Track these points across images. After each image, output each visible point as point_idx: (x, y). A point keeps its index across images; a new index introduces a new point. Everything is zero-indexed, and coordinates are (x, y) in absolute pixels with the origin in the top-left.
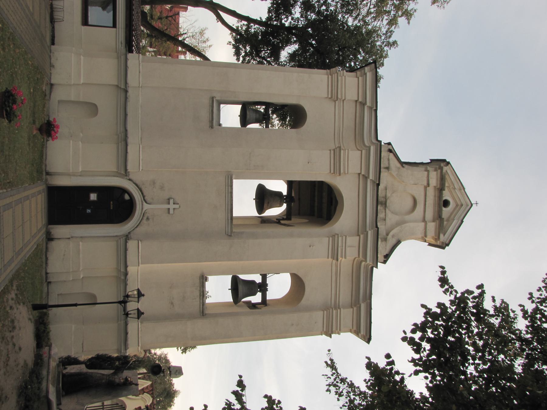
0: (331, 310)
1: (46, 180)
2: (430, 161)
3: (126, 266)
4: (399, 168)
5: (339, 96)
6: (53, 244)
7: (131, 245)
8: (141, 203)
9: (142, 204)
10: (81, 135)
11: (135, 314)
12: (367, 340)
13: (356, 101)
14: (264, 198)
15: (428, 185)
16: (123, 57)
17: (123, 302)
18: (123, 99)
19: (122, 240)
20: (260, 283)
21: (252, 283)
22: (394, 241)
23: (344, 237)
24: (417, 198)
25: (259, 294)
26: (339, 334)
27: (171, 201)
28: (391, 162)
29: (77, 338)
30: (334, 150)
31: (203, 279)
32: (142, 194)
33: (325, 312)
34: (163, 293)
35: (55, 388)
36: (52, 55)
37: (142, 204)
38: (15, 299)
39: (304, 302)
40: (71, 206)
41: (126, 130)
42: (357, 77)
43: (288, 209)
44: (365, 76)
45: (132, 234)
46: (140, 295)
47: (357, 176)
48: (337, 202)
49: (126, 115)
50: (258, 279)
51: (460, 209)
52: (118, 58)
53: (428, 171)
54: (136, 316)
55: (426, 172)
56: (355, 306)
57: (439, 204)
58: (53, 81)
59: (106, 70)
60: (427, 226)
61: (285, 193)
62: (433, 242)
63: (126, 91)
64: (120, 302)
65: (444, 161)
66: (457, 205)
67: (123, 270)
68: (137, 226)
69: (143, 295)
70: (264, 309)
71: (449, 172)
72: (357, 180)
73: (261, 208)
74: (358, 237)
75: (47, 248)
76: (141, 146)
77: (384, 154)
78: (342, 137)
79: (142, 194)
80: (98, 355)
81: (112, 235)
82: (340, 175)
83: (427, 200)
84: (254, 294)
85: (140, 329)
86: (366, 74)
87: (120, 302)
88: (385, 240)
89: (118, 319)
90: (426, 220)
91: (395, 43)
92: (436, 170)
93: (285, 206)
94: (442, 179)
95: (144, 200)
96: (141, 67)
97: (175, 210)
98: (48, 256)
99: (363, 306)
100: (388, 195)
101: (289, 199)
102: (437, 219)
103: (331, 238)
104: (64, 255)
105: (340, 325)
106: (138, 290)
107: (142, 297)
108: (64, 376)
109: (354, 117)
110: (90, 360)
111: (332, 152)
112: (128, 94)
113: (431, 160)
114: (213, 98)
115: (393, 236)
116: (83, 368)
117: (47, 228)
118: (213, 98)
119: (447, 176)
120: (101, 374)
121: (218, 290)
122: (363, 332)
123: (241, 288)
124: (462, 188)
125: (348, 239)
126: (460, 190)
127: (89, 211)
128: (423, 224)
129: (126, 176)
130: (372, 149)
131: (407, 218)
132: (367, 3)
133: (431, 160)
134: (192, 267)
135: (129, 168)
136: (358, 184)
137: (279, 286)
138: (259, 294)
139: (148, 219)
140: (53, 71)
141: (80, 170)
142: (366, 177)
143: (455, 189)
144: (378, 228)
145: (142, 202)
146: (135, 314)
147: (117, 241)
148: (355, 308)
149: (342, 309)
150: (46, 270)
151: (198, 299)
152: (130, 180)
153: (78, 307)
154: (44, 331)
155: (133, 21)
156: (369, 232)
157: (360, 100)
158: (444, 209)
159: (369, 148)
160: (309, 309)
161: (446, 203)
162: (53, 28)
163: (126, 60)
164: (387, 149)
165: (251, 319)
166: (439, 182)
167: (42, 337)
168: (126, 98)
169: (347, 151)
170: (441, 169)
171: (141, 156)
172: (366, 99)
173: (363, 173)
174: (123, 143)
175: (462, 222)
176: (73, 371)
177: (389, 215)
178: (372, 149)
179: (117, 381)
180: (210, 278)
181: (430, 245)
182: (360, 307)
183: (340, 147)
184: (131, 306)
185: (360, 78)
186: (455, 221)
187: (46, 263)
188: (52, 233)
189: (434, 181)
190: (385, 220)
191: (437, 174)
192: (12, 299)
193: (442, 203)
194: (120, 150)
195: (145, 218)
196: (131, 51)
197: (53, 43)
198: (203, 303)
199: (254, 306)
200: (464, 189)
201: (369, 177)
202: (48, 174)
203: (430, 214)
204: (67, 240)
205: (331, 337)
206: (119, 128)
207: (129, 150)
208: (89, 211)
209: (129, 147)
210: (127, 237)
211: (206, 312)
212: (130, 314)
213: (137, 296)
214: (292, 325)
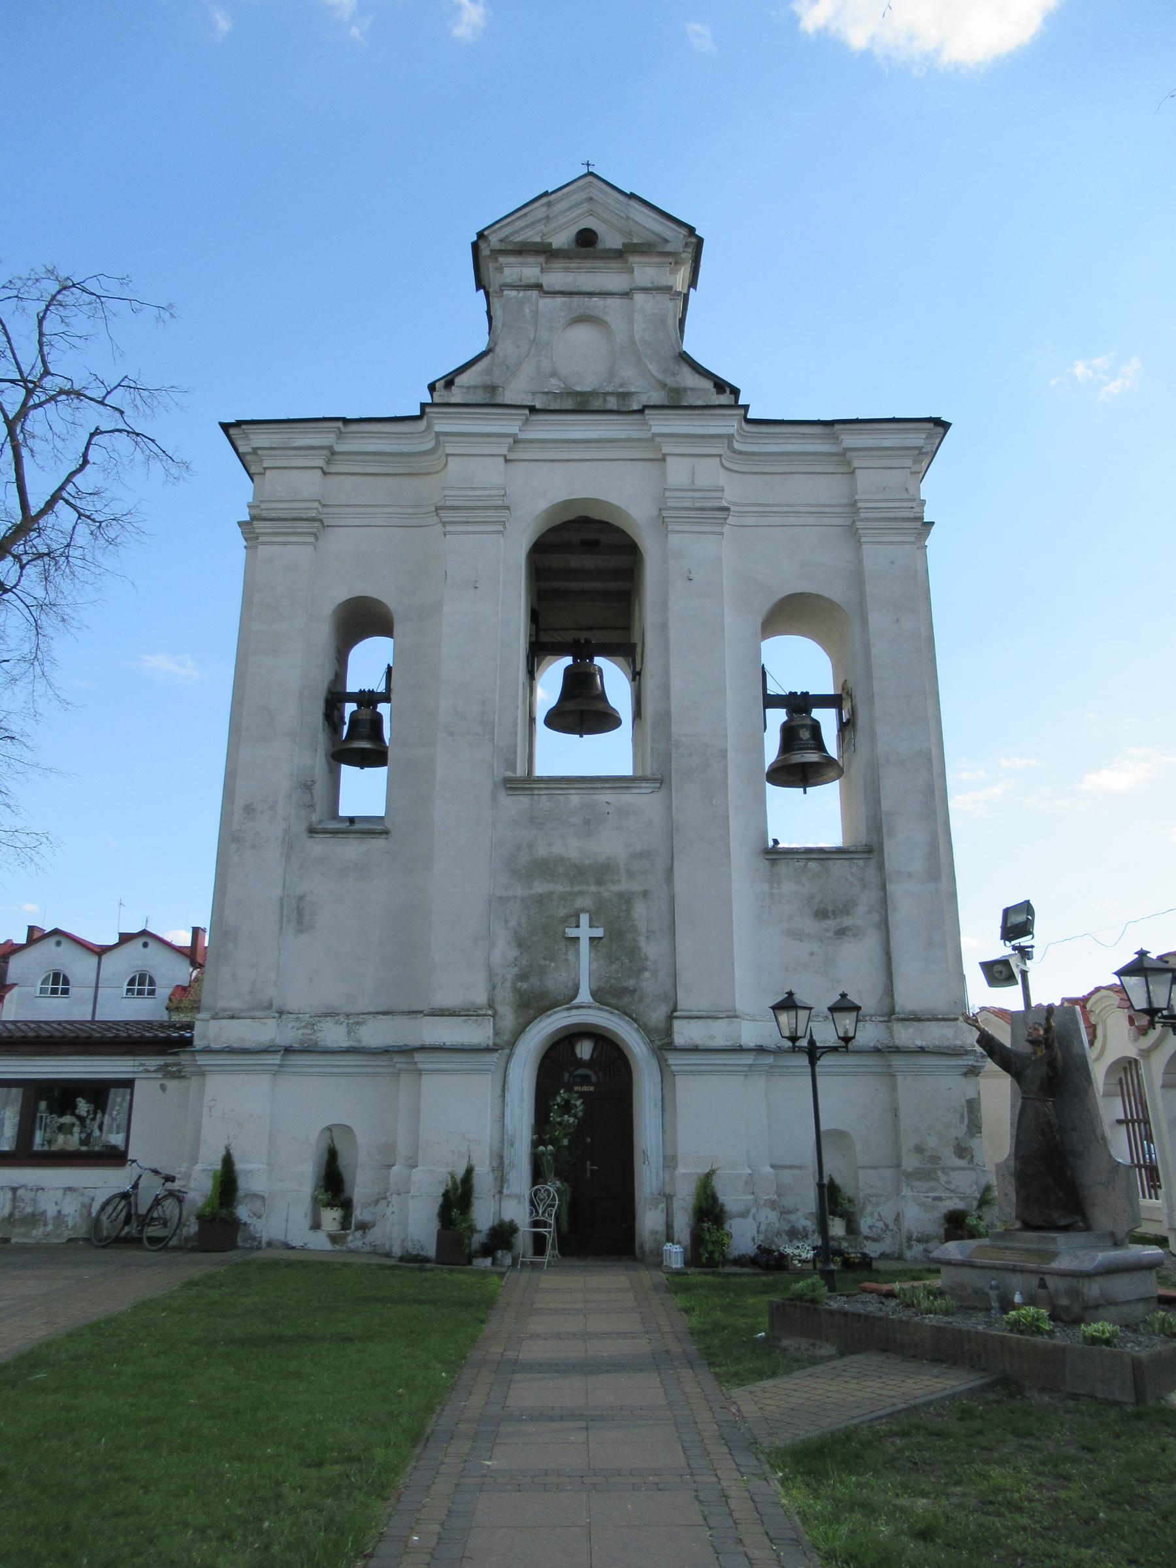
3: (740, 1050)
8: (574, 1012)
12: (941, 430)
14: (582, 711)
16: (202, 1060)
17: (813, 1052)
21: (789, 735)
25: (817, 714)
30: (444, 524)
31: (774, 854)
39: (836, 592)
42: (264, 474)
43: (608, 651)
44: (260, 452)
46: (788, 1004)
47: (511, 465)
48: (585, 521)
50: (777, 717)
56: (849, 463)
61: (568, 661)
64: (813, 1063)
65: (475, 247)
66: (591, 213)
67: (749, 1059)
69: (790, 994)
71: (501, 235)
73: (604, 720)
74: (669, 459)
77: (456, 396)
80: (362, 768)
82: (508, 508)
84: (816, 728)
86: (255, 450)
87: (813, 1063)
92: (500, 269)
93: (599, 661)
94: (523, 250)
99: (850, 440)
101: (583, 652)
102: (626, 261)
105: (894, 500)
106: (778, 1008)
107: (797, 997)
111: (449, 528)
113: (477, 290)
119: (518, 239)
121: (810, 818)
122: (917, 439)
124: (544, 200)
126: (549, 204)
128: (638, 297)
130: (441, 426)
133: (477, 290)
134: (743, 881)
136: (532, 464)
137: (800, 664)
138: (817, 714)
140: (311, 1246)
143: (547, 218)
155: (129, 1036)
157: (320, 463)
159: (438, 434)
160: (858, 578)
161: (586, 239)
163: (207, 1051)
164: (443, 392)
165: (887, 736)
169: (446, 492)
170: (496, 253)
173: (504, 451)
174: (418, 1057)
175: (632, 196)
178: (441, 426)
184: (825, 1034)
185: (266, 464)
189: (530, 270)
191: (510, 265)
194: (443, 1066)
196: (189, 1042)
198: (839, 851)
199: (845, 727)
200: (546, 194)
201: (514, 436)
203: (612, 280)
213: (793, 1013)
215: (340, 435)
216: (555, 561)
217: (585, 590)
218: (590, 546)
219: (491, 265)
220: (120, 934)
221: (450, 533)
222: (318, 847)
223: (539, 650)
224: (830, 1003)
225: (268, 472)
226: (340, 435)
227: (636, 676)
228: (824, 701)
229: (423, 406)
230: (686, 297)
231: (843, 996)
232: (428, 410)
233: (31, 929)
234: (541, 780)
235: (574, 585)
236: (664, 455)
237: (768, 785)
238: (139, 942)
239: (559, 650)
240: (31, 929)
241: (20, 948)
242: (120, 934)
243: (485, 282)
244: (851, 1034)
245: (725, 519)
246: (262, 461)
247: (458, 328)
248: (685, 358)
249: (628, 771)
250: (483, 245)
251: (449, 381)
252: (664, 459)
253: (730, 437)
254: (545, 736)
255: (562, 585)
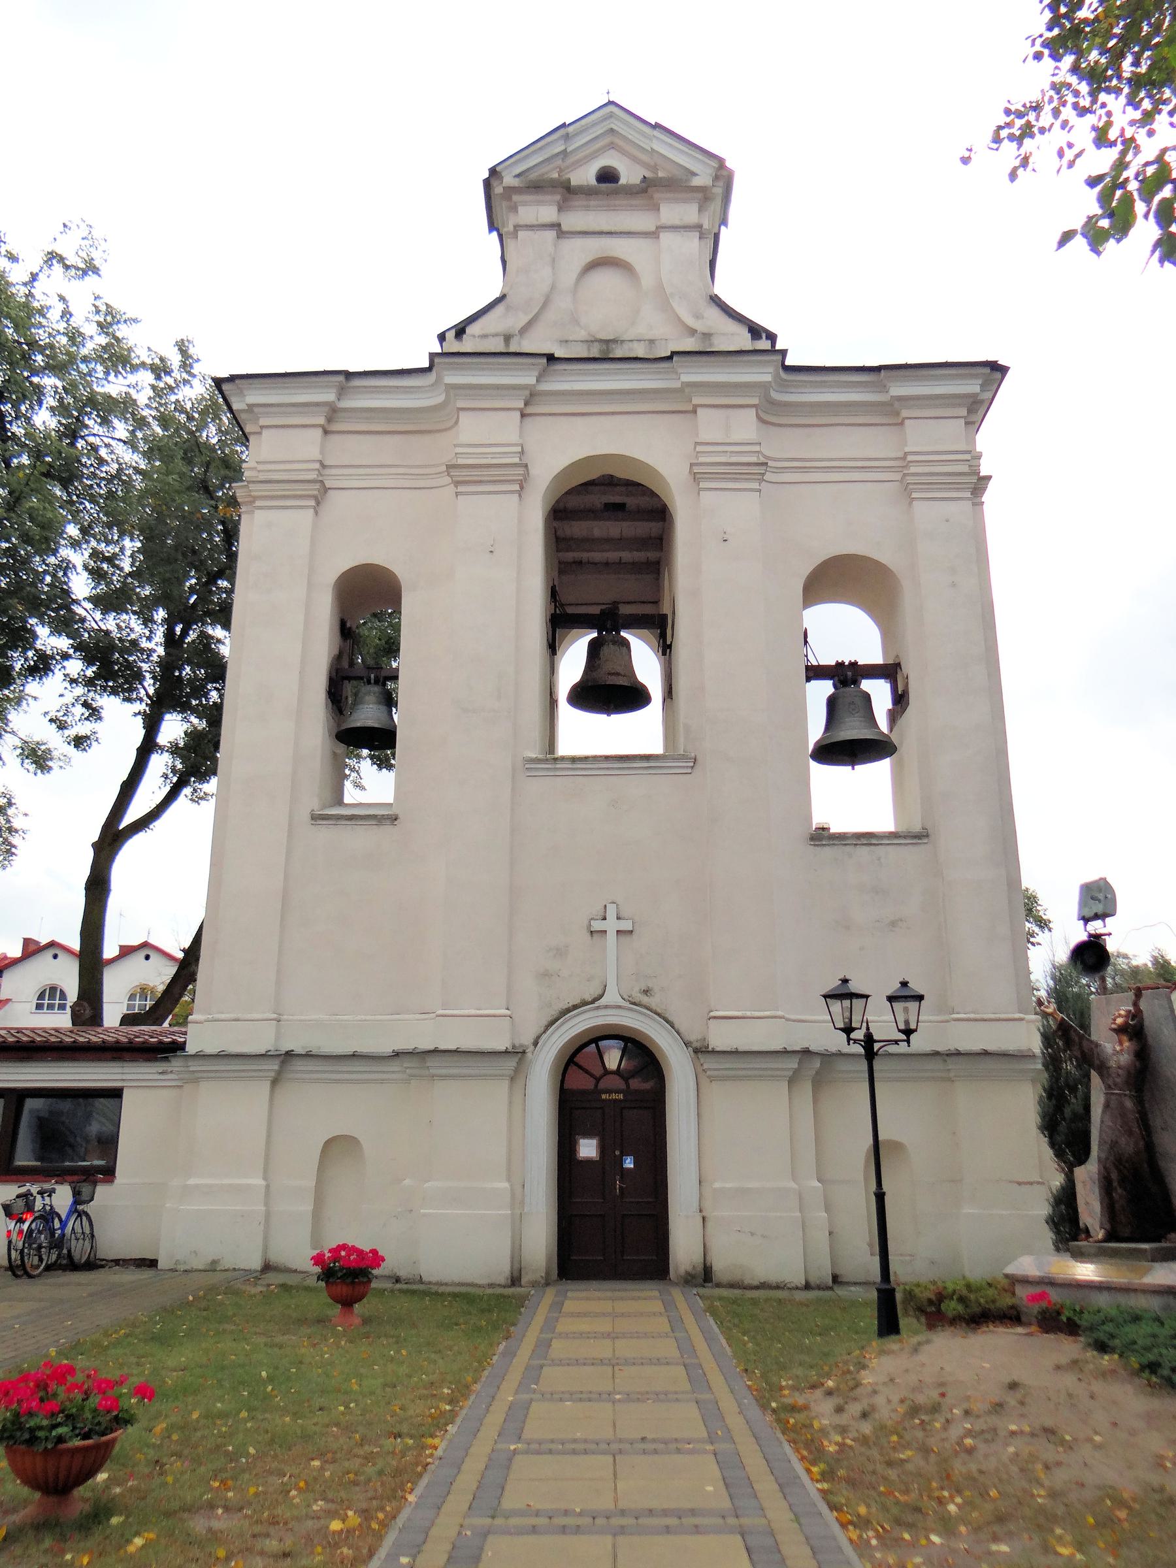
0: (910, 479)
1: (534, 1284)
2: (495, 234)
4: (508, 308)
5: (312, 476)
6: (720, 1265)
7: (721, 1038)
8: (596, 1013)
9: (606, 1007)
10: (407, 1182)
11: (906, 1010)
12: (998, 375)
13: (326, 432)
14: (609, 692)
15: (556, 226)
16: (195, 1066)
18: (311, 1065)
19: (709, 1063)
20: (835, 686)
22: (714, 313)
23: (699, 448)
24: (590, 258)
26: (979, 456)
27: (597, 925)
28: (492, 329)
29: (988, 1189)
30: (457, 483)
31: (822, 837)
32: (575, 1007)
33: (914, 495)
34: (862, 949)
35: (1157, 1265)
36: (182, 1267)
37: (606, 1007)
38: (840, 1401)
40: (612, 1213)
41: (397, 1054)
42: (260, 433)
43: (637, 622)
44: (256, 410)
45: (693, 1037)
46: (843, 994)
47: (528, 420)
48: (609, 482)
49: (354, 1056)
50: (825, 688)
51: (625, 138)
52: (196, 1081)
53: (517, 227)
54: (913, 1006)
55: (521, 234)
56: (898, 414)
57: (608, 194)
58: (256, 1264)
59: (230, 1113)
60: (669, 223)
62: (716, 205)
63: (289, 1054)
65: (487, 184)
66: (612, 146)
68: (667, 1021)
70: (910, 669)
72: (538, 418)
73: (630, 697)
74: (699, 410)
75: (732, 1286)
76: (441, 1012)
77: (467, 345)
78: (426, 466)
79: (575, 1007)
81: (693, 1094)
83: (597, 229)
84: (867, 697)
85: (972, 1016)
86: (251, 407)
88: (707, 336)
89: (943, 1079)
90: (653, 229)
91: (183, 348)
92: (514, 209)
95: (593, 1002)
96: (223, 1016)
97: (621, 915)
98: (756, 1283)
99: (898, 389)
100: (583, 334)
102: (652, 197)
103: (702, 485)
104: (752, 1234)
108: (1111, 1236)
109: (368, 437)
110: (1059, 1154)
111: (461, 489)
112: (299, 1050)
113: (491, 231)
114: (316, 818)
115: (698, 316)
116: (1087, 1175)
117: (677, 1284)
118: (316, 818)
119: (533, 176)
120: (1104, 1112)
121: (854, 799)
122: (972, 387)
123: (852, 731)
124: (562, 132)
125: (704, 436)
126: (567, 137)
127: (629, 1163)
129: (524, 1052)
130: (451, 379)
131: (647, 281)
132: (107, 446)
133: (491, 231)
135: (501, 1043)
137: (844, 632)
138: (866, 685)
139: (646, 992)
140: (227, 1263)
141: (506, 1185)
142: (531, 395)
143: (564, 153)
144: (673, 353)
145: (598, 1008)
146: (906, 1010)
147: (712, 1079)
148: (905, 413)
149: (907, 449)
150: (797, 1288)
151: (880, 850)
152: (536, 1044)
153: (885, 1188)
154: (961, 1299)
155: (118, 1042)
156: (685, 378)
158: (623, 181)
161: (607, 176)
162: (117, 1262)
163: (200, 1056)
166: (548, 197)
167: (978, 1309)
168: (308, 1055)
170: (510, 191)
171: (466, 1012)
172: (317, 404)
174: (431, 1062)
175: (657, 126)
176: (1097, 1206)
177: (641, 329)
178: (451, 379)
179: (1125, 1059)
180: (819, 818)
181: (724, 222)
182: (900, 399)
183: (449, 467)
184: (882, 1021)
185: (262, 422)
186: (656, 147)
187: (778, 1287)
188: (689, 1269)
190: (652, 341)
191: (525, 204)
192: (839, 1410)
193: (604, 186)
195: (645, 1000)
196: (181, 1047)
197: (152, 1263)
199: (900, 699)
200: (564, 125)
202: (515, 1280)
203: (640, 220)
204: (709, 1224)
205: (989, 478)
206: (394, 1076)
207: (452, 1047)
208: (629, 1163)
209: (442, 1047)
210: (701, 1051)
211: (917, 828)
212: (907, 1022)
213: (847, 1003)
214: (954, 585)
215: (342, 392)
216: (578, 529)
217: (609, 562)
218: (616, 509)
219: (505, 204)
220: (121, 947)
221: (462, 493)
222: (325, 834)
223: (561, 622)
224: (889, 992)
225: (265, 432)
226: (342, 392)
227: (665, 648)
228: (873, 672)
229: (432, 356)
230: (716, 237)
231: (904, 984)
232: (437, 360)
233: (27, 942)
234: (563, 758)
235: (597, 556)
236: (696, 407)
237: (813, 765)
238: (141, 955)
239: (584, 622)
240: (27, 942)
241: (15, 962)
242: (121, 947)
243: (497, 224)
244: (913, 1026)
245: (763, 474)
246: (258, 419)
247: (467, 271)
248: (716, 301)
249: (657, 748)
250: (494, 183)
251: (460, 331)
252: (695, 412)
253: (764, 386)
254: (566, 711)
255: (584, 556)
